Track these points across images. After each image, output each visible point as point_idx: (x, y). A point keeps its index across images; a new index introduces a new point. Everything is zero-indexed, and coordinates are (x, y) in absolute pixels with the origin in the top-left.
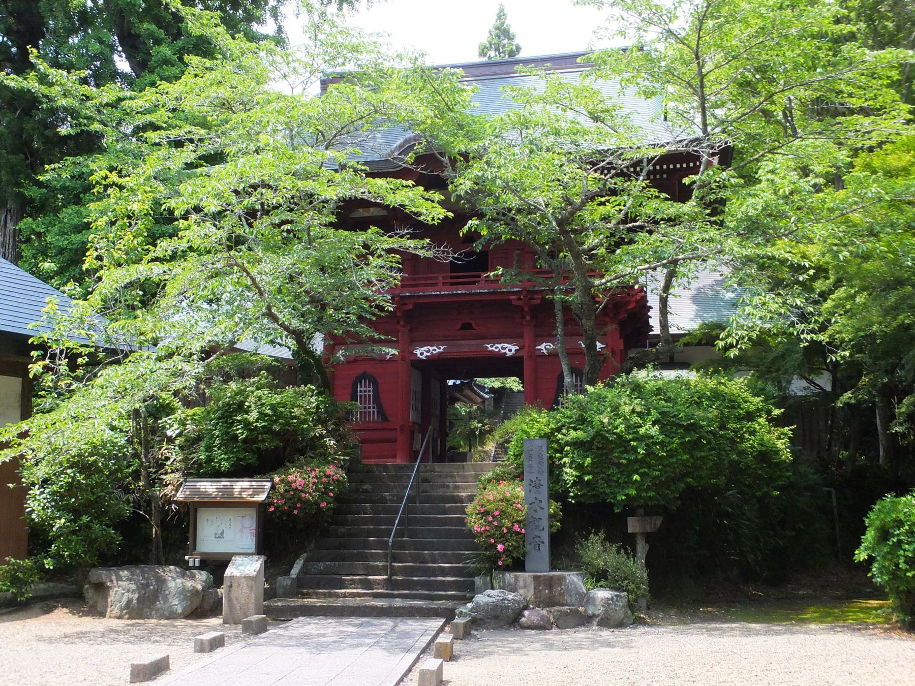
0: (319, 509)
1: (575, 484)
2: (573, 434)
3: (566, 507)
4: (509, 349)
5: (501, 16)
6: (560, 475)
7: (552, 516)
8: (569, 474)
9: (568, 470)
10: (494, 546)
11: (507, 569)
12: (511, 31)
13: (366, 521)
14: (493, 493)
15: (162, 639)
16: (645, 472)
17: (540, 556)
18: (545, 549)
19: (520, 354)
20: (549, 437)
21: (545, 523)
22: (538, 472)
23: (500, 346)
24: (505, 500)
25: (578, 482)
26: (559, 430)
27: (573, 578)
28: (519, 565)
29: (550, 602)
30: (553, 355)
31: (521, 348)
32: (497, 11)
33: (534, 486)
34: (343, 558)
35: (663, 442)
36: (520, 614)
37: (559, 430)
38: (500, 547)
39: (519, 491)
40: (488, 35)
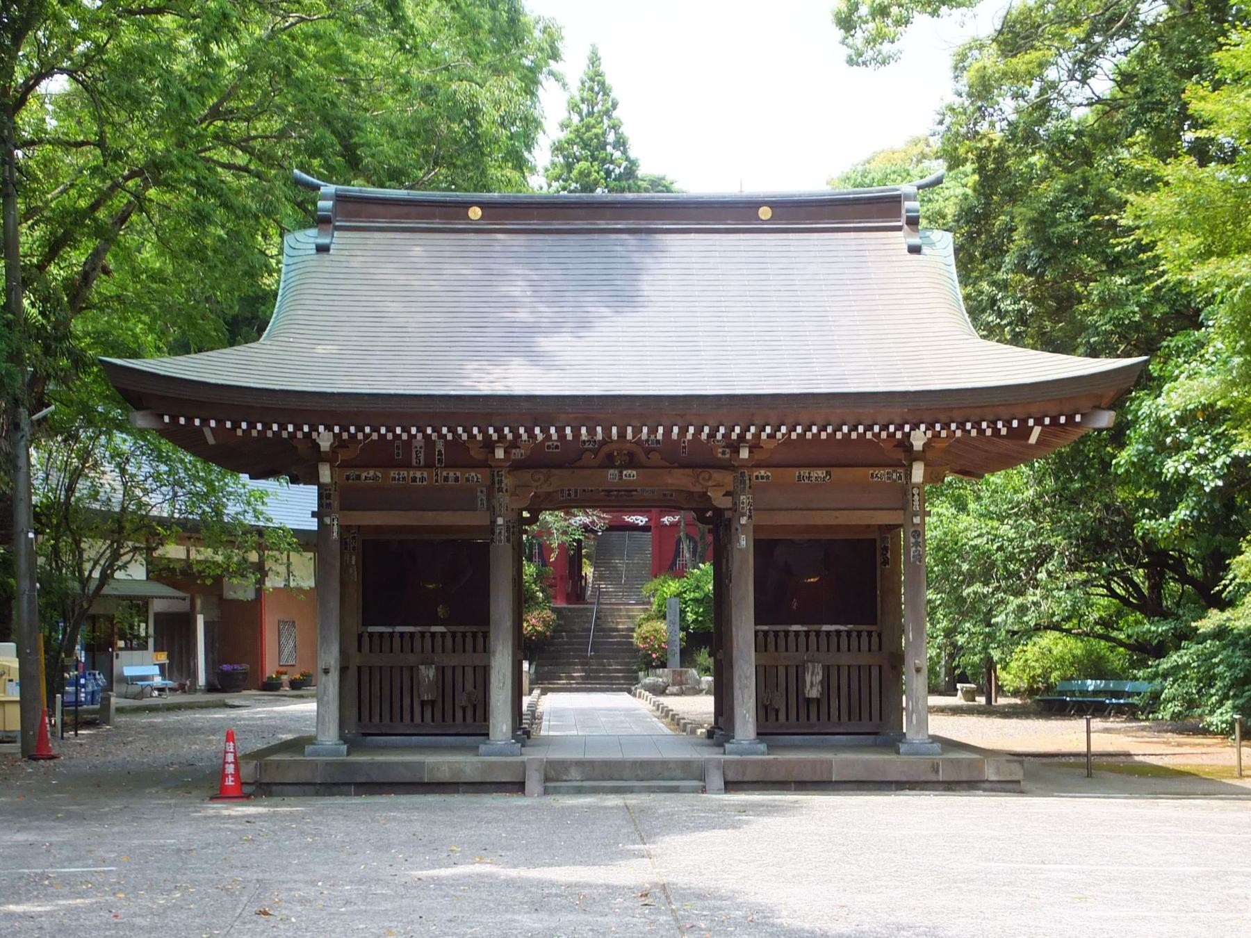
0: (546, 636)
1: (693, 622)
2: (692, 595)
3: (688, 633)
4: (641, 520)
5: (594, 60)
6: (685, 617)
7: (681, 639)
8: (690, 617)
9: (689, 614)
10: (651, 655)
11: (658, 667)
12: (607, 82)
13: (566, 643)
14: (647, 627)
15: (57, 824)
16: (1095, 220)
17: (675, 659)
18: (678, 656)
19: (649, 524)
20: (679, 595)
21: (678, 642)
22: (673, 615)
23: (634, 518)
24: (656, 630)
25: (695, 621)
26: (685, 592)
27: (694, 672)
28: (663, 665)
29: (681, 683)
30: (674, 526)
31: (650, 520)
32: (588, 53)
33: (672, 623)
34: (557, 665)
35: (1069, 189)
36: (666, 689)
37: (685, 592)
38: (654, 656)
39: (662, 626)
40: (580, 85)
